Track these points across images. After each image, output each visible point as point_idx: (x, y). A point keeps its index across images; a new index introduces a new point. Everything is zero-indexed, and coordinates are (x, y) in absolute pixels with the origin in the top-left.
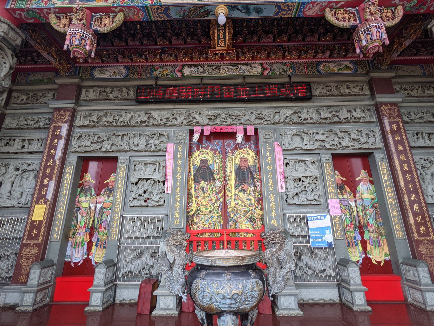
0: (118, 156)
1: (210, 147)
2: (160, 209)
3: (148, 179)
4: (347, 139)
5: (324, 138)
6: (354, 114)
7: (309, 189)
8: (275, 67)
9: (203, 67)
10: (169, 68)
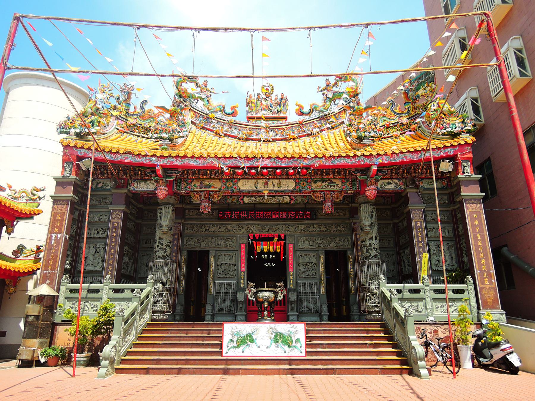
0: (209, 251)
1: (45, 272)
2: (233, 279)
3: (226, 263)
4: (333, 243)
5: (321, 242)
6: (339, 228)
7: (311, 270)
8: (297, 198)
9: (255, 197)
10: (235, 197)
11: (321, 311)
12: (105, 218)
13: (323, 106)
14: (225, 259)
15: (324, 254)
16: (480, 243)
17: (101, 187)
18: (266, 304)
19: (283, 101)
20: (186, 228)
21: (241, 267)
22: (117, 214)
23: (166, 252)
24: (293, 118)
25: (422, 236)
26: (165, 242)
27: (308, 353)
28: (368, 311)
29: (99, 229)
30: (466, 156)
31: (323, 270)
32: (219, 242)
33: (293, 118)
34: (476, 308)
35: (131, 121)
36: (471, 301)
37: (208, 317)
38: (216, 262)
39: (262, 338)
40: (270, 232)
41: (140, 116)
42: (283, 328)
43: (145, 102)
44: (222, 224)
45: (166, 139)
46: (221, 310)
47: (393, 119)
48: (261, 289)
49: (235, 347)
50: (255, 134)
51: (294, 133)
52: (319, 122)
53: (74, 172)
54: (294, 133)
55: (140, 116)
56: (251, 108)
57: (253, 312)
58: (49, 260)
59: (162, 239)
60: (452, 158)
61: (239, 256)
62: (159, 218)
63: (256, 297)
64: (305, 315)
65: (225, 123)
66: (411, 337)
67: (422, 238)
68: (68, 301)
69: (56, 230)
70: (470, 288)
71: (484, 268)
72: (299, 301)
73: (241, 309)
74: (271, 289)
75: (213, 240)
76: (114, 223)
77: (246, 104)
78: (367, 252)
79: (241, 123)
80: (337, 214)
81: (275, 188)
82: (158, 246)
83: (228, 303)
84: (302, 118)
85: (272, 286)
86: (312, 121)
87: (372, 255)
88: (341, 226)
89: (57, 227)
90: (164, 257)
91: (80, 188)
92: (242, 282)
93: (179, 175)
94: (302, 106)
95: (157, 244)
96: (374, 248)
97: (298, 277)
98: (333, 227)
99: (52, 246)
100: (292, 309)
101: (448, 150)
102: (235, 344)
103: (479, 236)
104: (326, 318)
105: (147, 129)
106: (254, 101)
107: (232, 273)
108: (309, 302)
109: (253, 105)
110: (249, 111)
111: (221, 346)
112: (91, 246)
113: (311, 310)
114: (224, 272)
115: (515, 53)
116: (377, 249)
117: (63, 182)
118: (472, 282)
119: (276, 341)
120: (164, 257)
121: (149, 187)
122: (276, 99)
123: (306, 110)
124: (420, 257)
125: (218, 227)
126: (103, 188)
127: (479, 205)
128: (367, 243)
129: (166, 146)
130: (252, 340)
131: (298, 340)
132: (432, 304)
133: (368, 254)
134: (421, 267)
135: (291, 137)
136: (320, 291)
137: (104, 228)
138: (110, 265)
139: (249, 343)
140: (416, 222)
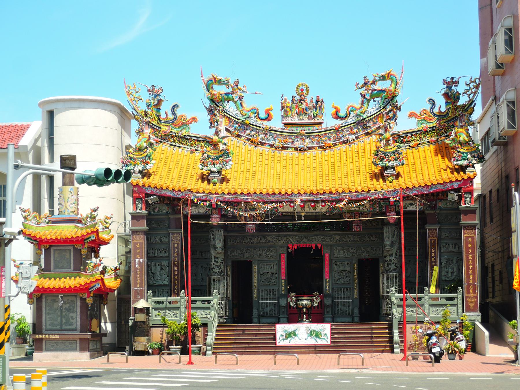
3: (268, 272)
4: (366, 252)
5: (355, 251)
6: (371, 238)
11: (353, 313)
12: (165, 240)
13: (361, 108)
14: (266, 269)
15: (357, 262)
16: (470, 262)
17: (158, 212)
18: (305, 310)
19: (318, 105)
20: (229, 240)
21: (282, 276)
22: (176, 236)
23: (221, 268)
24: (329, 122)
25: (435, 252)
26: (219, 261)
27: (332, 342)
28: (386, 314)
29: (161, 249)
30: (468, 189)
31: (356, 277)
32: (261, 253)
33: (329, 122)
34: (461, 311)
35: (165, 128)
36: (459, 306)
37: (255, 320)
38: (258, 271)
39: (303, 333)
40: (308, 243)
41: (173, 122)
42: (315, 327)
43: (175, 107)
44: (263, 235)
45: (215, 172)
46: (266, 313)
47: (431, 123)
48: (300, 298)
49: (284, 339)
50: (291, 141)
51: (330, 140)
52: (355, 126)
53: (144, 207)
54: (330, 140)
55: (173, 122)
56: (286, 112)
57: (294, 316)
58: (137, 280)
59: (217, 258)
60: (458, 190)
61: (279, 266)
62: (212, 239)
63: (296, 304)
64: (339, 317)
65: (260, 130)
66: (394, 331)
67: (435, 254)
68: (155, 310)
69: (138, 256)
70: (459, 296)
71: (471, 281)
72: (334, 305)
73: (283, 313)
74: (308, 298)
75: (255, 251)
76: (174, 244)
77: (280, 108)
78: (388, 266)
79: (276, 129)
80: (371, 225)
81: (310, 211)
82: (214, 264)
83: (272, 307)
84: (338, 123)
85: (309, 294)
86: (348, 127)
87: (392, 269)
88: (374, 236)
89: (138, 254)
90: (220, 273)
91: (150, 219)
92: (283, 288)
93: (229, 210)
94: (339, 108)
95: (213, 262)
96: (393, 263)
97: (333, 283)
98: (366, 237)
99: (137, 269)
100: (328, 312)
101: (454, 184)
102: (284, 338)
103: (470, 256)
104: (357, 319)
105: (181, 137)
106: (288, 105)
107: (273, 281)
108: (344, 305)
109: (288, 110)
110: (285, 115)
111: (275, 339)
112: (157, 264)
113: (345, 313)
114: (268, 280)
115: (508, 105)
116: (396, 264)
117: (136, 216)
118: (461, 292)
119: (311, 335)
120: (220, 273)
121: (200, 211)
122: (312, 102)
123: (342, 114)
124: (431, 269)
125: (259, 239)
126: (160, 213)
127: (474, 231)
128: (388, 259)
129: (216, 180)
130: (295, 335)
131: (325, 334)
132: (429, 308)
133: (388, 268)
134: (432, 278)
135: (327, 145)
136: (353, 297)
137: (165, 248)
138: (176, 280)
139: (293, 337)
140: (431, 240)
